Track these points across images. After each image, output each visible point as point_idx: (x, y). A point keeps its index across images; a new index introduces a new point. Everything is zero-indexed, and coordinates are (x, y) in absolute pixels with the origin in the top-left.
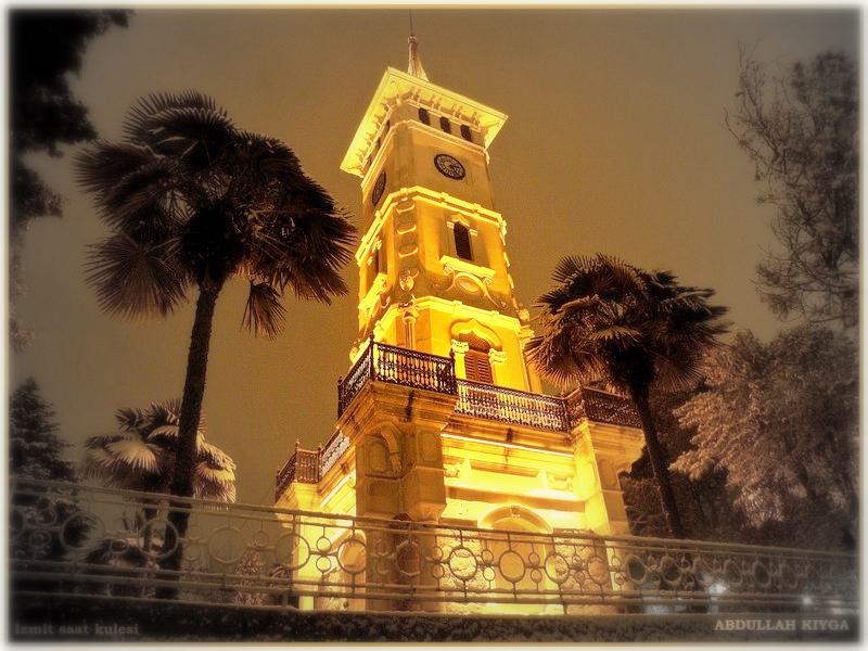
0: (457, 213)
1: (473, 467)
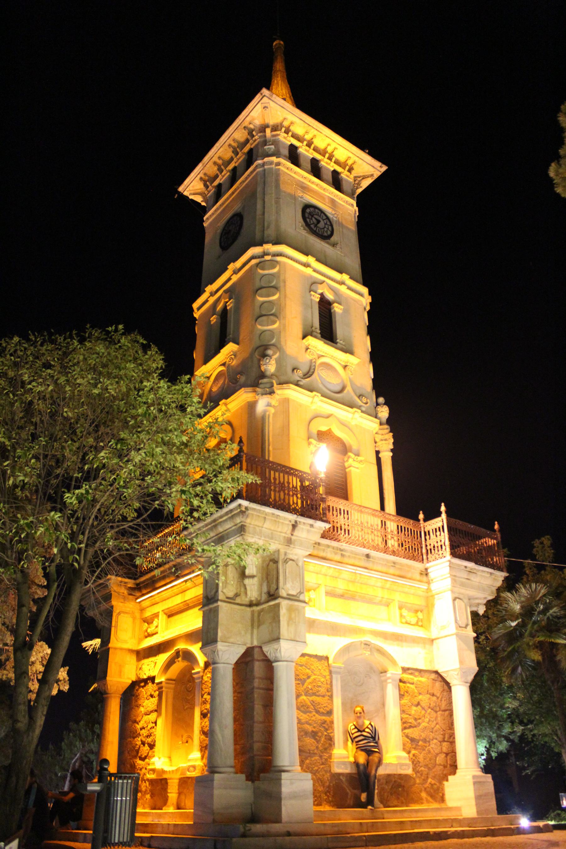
0: (322, 282)
1: (328, 594)
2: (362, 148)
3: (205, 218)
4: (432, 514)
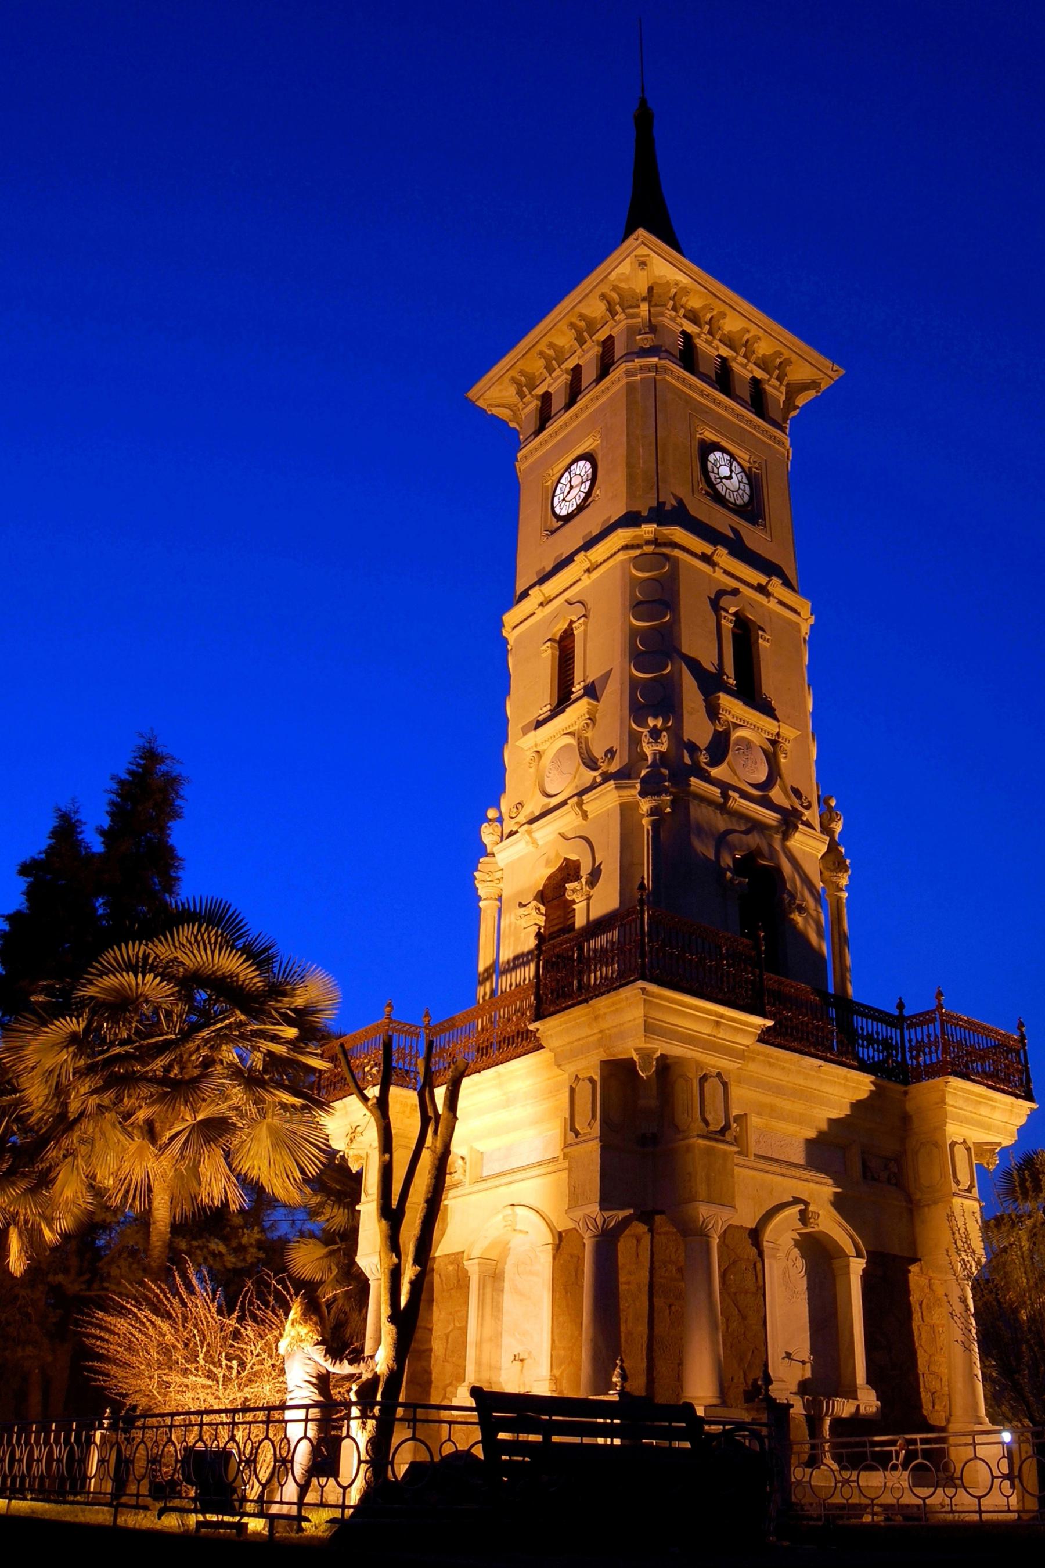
0: (735, 592)
3: (519, 455)
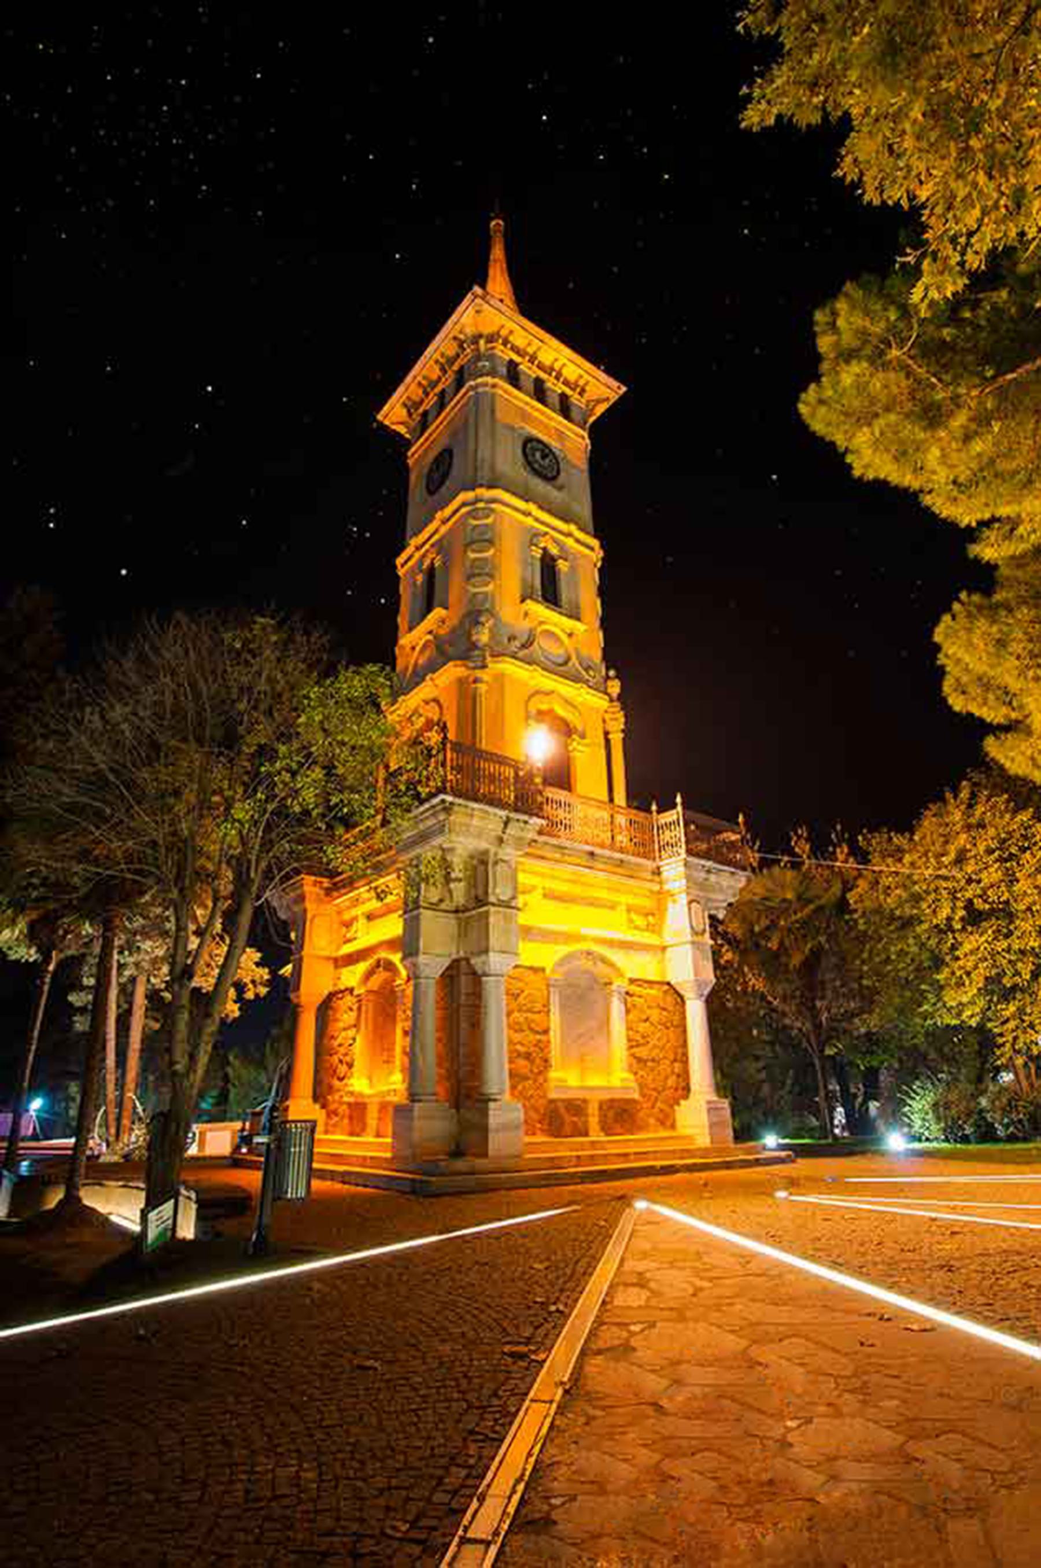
1: (545, 896)
2: (596, 363)
4: (667, 805)
